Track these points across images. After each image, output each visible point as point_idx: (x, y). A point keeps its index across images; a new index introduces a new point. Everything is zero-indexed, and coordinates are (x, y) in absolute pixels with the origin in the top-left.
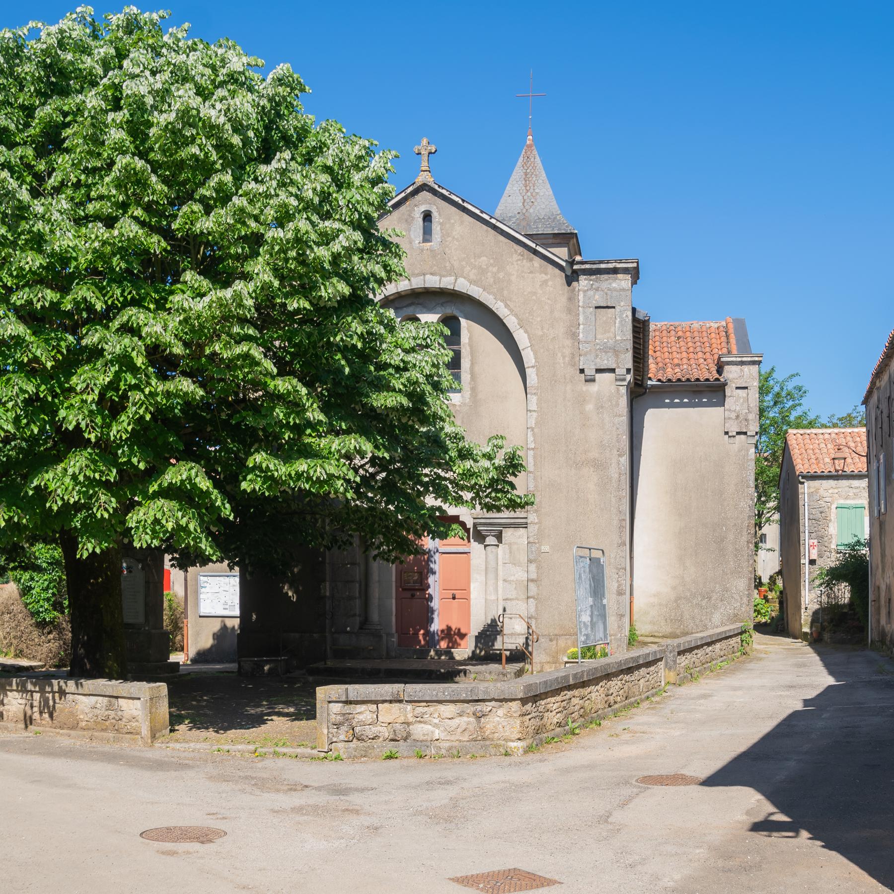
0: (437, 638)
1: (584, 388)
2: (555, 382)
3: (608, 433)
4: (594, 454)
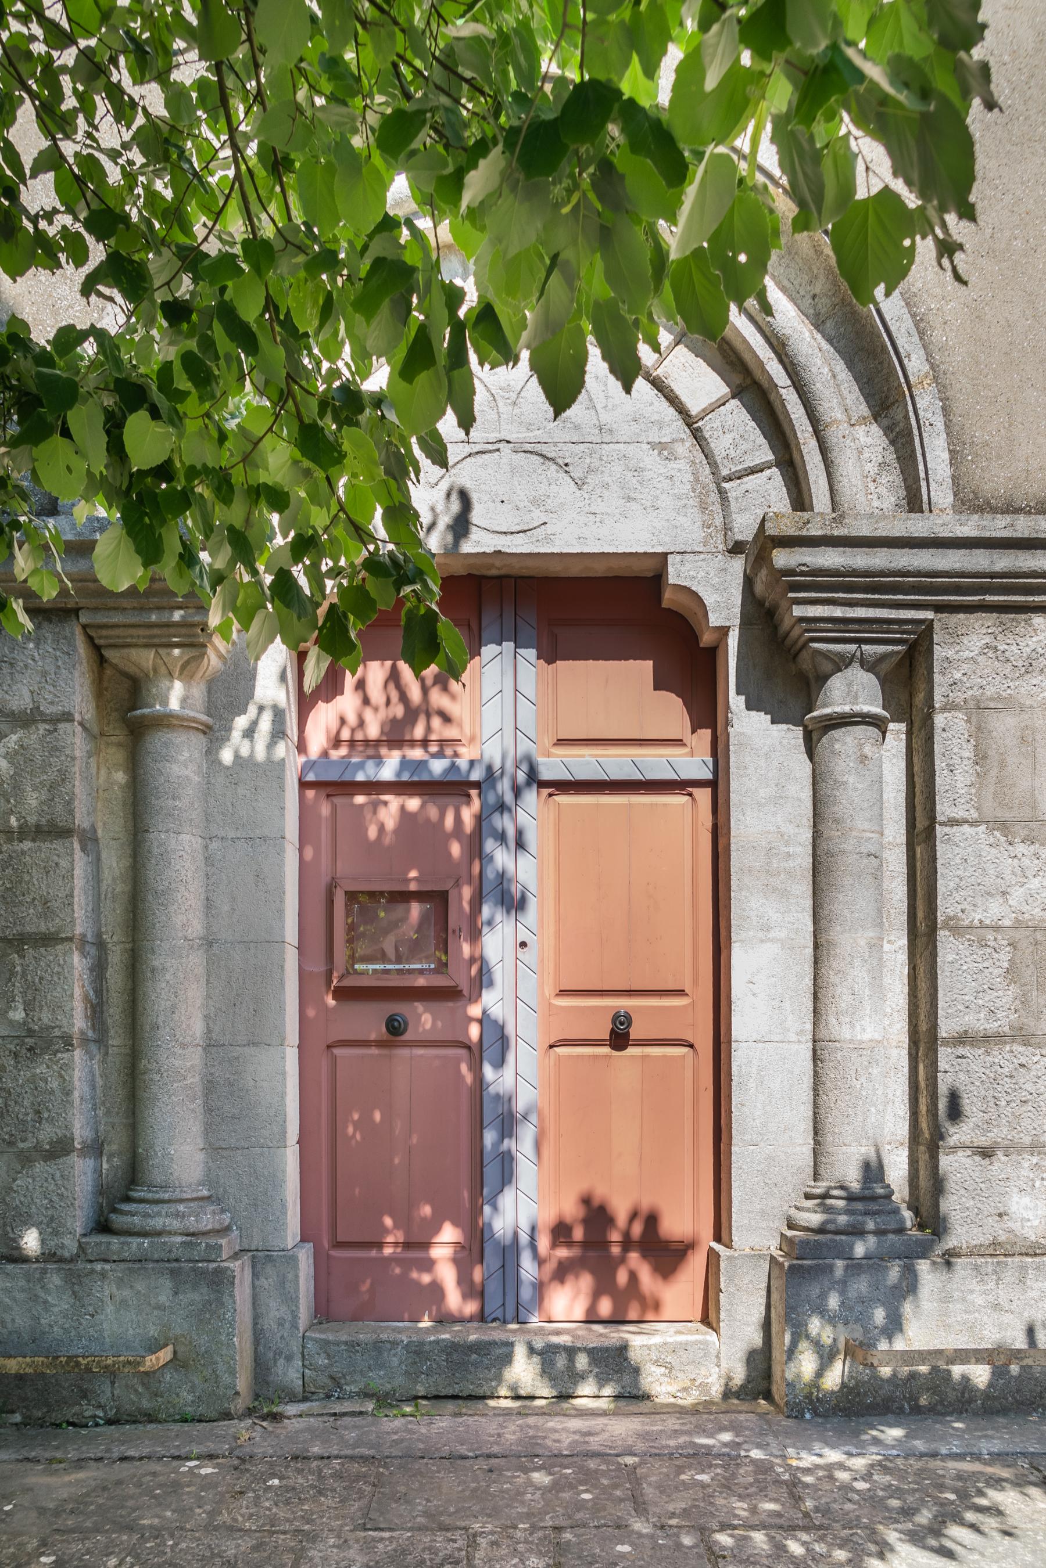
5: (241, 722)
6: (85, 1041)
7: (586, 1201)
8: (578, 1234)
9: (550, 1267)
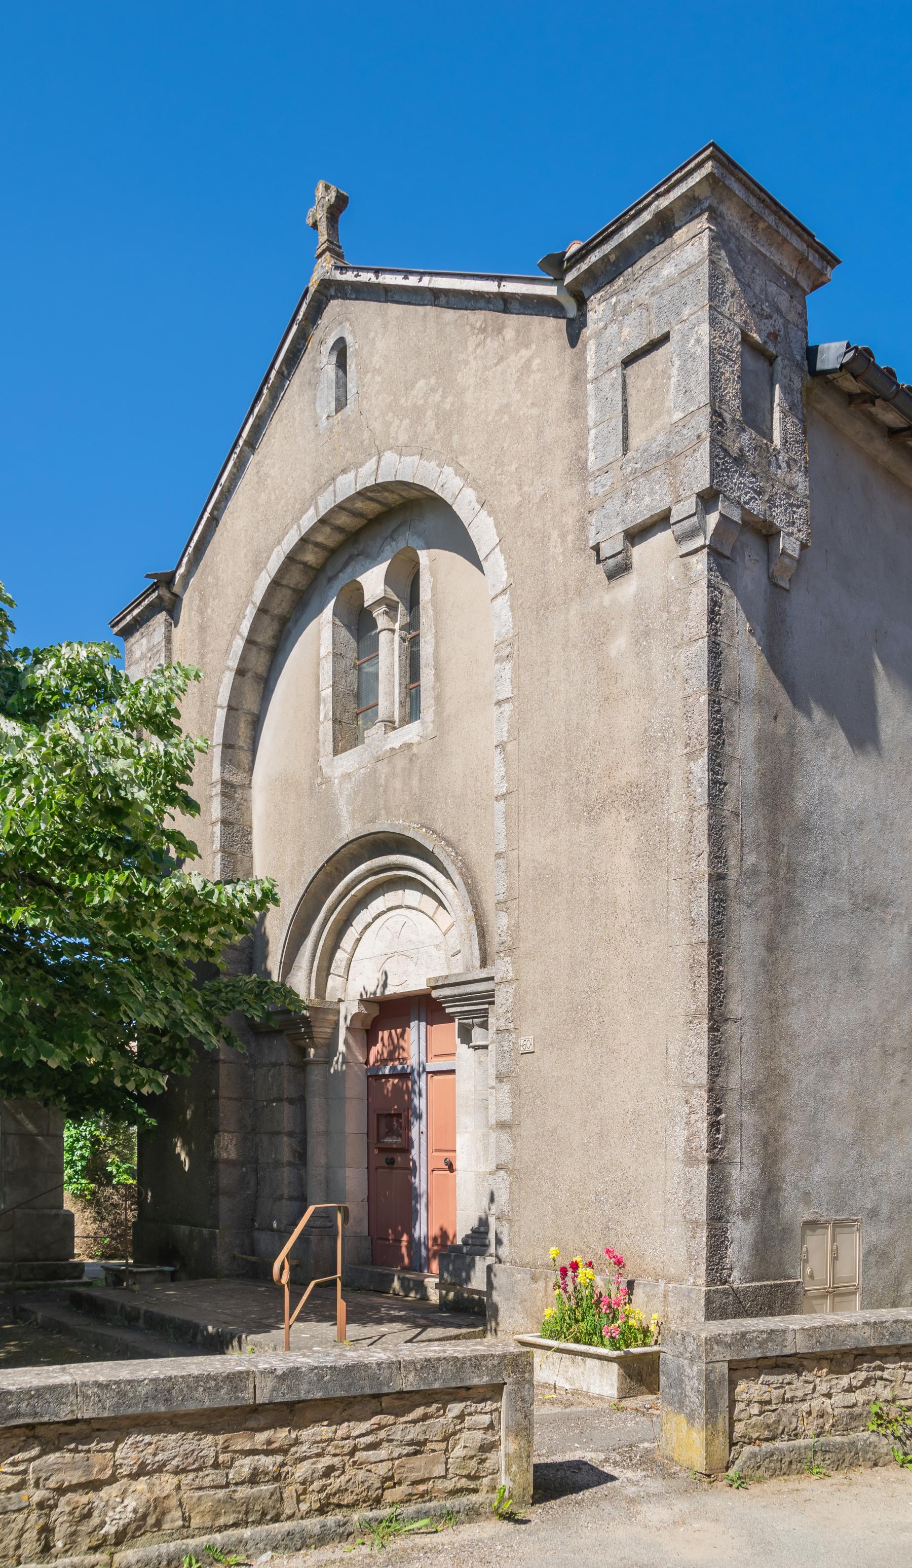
0: (424, 1252)
1: (607, 599)
2: (547, 608)
3: (661, 701)
4: (629, 772)
5: (335, 1059)
6: (290, 1164)
7: (441, 1229)
8: (439, 1241)
9: (431, 1253)
